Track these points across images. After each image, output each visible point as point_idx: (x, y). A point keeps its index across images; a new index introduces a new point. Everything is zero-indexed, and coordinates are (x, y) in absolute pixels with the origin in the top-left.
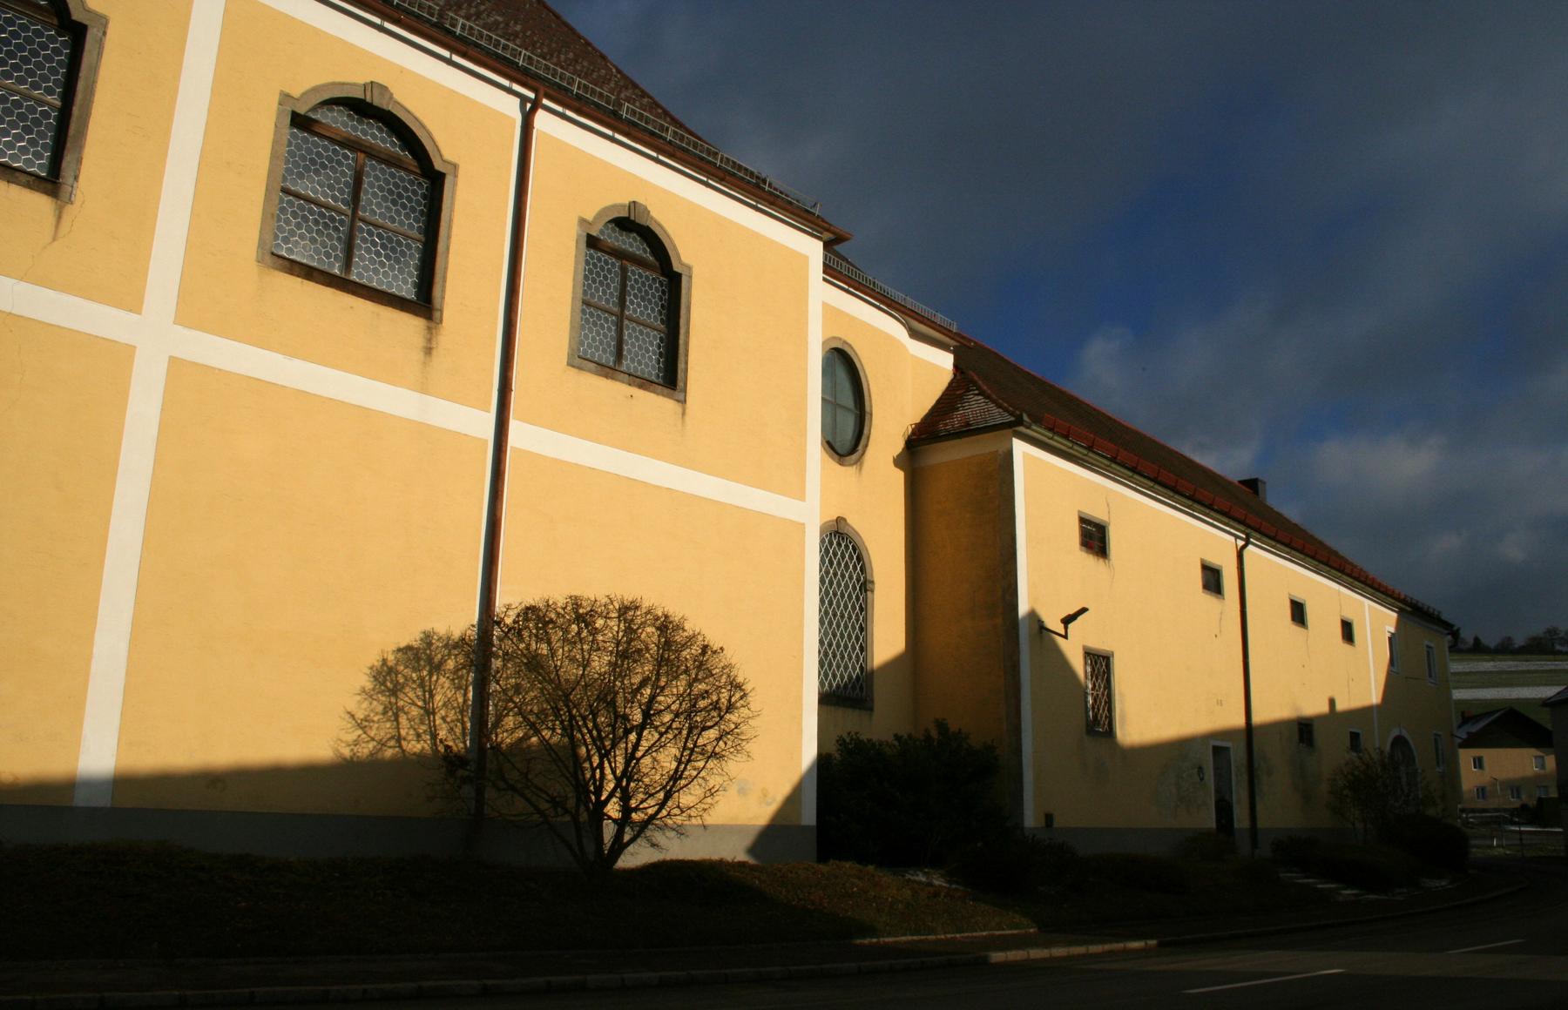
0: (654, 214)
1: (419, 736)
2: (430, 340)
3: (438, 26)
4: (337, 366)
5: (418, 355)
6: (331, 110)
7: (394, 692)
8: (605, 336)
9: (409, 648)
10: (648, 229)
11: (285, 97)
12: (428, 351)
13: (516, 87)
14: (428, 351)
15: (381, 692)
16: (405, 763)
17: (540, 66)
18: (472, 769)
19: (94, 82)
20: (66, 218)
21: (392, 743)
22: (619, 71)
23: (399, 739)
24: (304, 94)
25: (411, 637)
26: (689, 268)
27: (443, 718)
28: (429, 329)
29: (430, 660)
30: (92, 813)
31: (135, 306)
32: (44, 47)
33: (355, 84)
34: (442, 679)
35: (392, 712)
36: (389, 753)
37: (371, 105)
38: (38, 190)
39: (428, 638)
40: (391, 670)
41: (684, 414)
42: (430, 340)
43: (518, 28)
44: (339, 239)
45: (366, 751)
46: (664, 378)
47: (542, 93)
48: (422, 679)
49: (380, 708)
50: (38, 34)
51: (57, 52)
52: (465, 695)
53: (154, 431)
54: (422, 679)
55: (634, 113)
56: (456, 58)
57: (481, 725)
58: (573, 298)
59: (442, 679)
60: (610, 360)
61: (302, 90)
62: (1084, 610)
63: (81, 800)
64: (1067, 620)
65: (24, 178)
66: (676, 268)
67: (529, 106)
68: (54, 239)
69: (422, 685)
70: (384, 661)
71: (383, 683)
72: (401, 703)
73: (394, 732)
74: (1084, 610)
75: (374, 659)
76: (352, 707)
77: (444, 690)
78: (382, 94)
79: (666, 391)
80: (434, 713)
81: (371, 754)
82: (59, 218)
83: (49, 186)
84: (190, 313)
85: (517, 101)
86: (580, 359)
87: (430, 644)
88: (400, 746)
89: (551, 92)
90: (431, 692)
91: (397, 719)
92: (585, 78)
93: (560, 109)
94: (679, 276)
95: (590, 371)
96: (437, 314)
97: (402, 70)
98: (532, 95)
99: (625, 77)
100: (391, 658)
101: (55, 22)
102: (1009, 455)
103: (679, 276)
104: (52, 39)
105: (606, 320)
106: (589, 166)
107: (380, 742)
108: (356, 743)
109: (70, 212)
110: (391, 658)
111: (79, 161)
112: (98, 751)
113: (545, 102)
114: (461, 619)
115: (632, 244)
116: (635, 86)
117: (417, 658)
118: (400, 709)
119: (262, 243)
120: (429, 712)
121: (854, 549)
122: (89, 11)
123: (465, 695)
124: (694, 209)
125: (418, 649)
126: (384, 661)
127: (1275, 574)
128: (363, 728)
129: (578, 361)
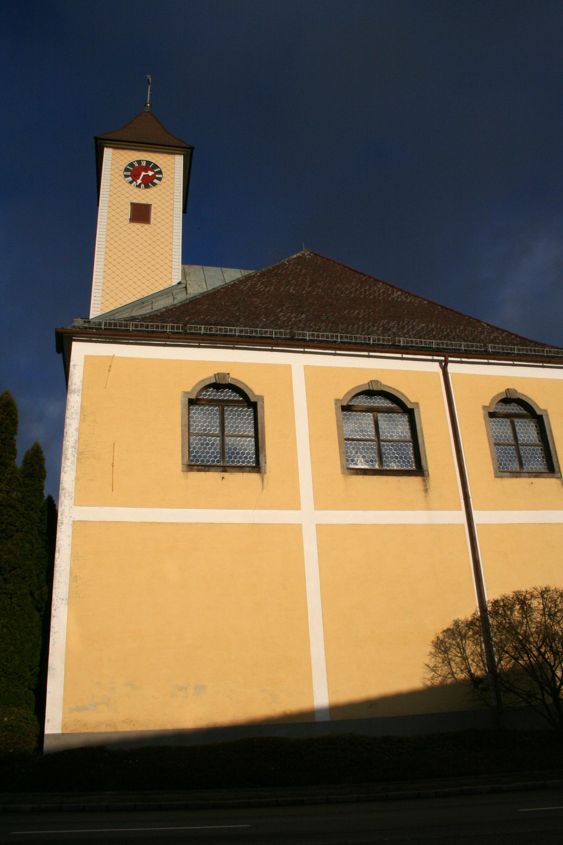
0: (520, 391)
1: (462, 670)
2: (425, 486)
5: (421, 494)
6: (358, 399)
7: (446, 651)
8: (512, 457)
9: (449, 630)
10: (519, 399)
11: (337, 401)
12: (426, 490)
13: (435, 358)
14: (426, 490)
15: (440, 653)
16: (457, 684)
17: (445, 344)
18: (488, 687)
19: (264, 423)
21: (450, 676)
22: (488, 325)
23: (453, 674)
25: (448, 624)
26: (545, 411)
27: (473, 660)
28: (424, 481)
29: (460, 633)
30: (324, 724)
31: (298, 507)
32: (244, 415)
33: (364, 385)
34: (468, 642)
35: (448, 661)
36: (449, 681)
37: (373, 391)
38: (254, 472)
39: (456, 623)
40: (442, 642)
42: (425, 486)
43: (433, 325)
44: (375, 453)
45: (438, 682)
46: (548, 468)
47: (447, 356)
48: (458, 643)
49: (441, 660)
50: (241, 411)
51: (249, 415)
52: (481, 647)
53: (316, 557)
54: (458, 643)
55: (495, 347)
57: (491, 664)
59: (468, 642)
60: (516, 466)
61: (343, 395)
63: (318, 719)
65: (247, 469)
66: (539, 413)
67: (443, 364)
68: (263, 489)
69: (458, 646)
70: (438, 638)
71: (440, 648)
72: (450, 656)
73: (449, 671)
75: (433, 638)
76: (427, 662)
77: (470, 647)
78: (376, 384)
79: (549, 475)
80: (467, 659)
81: (441, 683)
83: (257, 469)
84: (321, 503)
85: (438, 364)
86: (502, 470)
87: (458, 626)
88: (454, 677)
89: (451, 354)
90: (463, 649)
91: (450, 664)
94: (541, 417)
95: (507, 477)
96: (426, 473)
97: (383, 370)
98: (443, 358)
99: (492, 327)
100: (441, 636)
101: (246, 404)
103: (541, 417)
104: (246, 411)
105: (510, 450)
106: (482, 379)
107: (444, 676)
108: (432, 678)
109: (266, 477)
110: (441, 636)
111: (265, 455)
112: (321, 698)
113: (450, 359)
115: (514, 409)
116: (498, 329)
117: (454, 634)
118: (451, 659)
119: (342, 466)
120: (465, 659)
122: (256, 396)
123: (481, 647)
124: (539, 381)
125: (453, 629)
126: (438, 638)
128: (434, 671)
129: (500, 474)
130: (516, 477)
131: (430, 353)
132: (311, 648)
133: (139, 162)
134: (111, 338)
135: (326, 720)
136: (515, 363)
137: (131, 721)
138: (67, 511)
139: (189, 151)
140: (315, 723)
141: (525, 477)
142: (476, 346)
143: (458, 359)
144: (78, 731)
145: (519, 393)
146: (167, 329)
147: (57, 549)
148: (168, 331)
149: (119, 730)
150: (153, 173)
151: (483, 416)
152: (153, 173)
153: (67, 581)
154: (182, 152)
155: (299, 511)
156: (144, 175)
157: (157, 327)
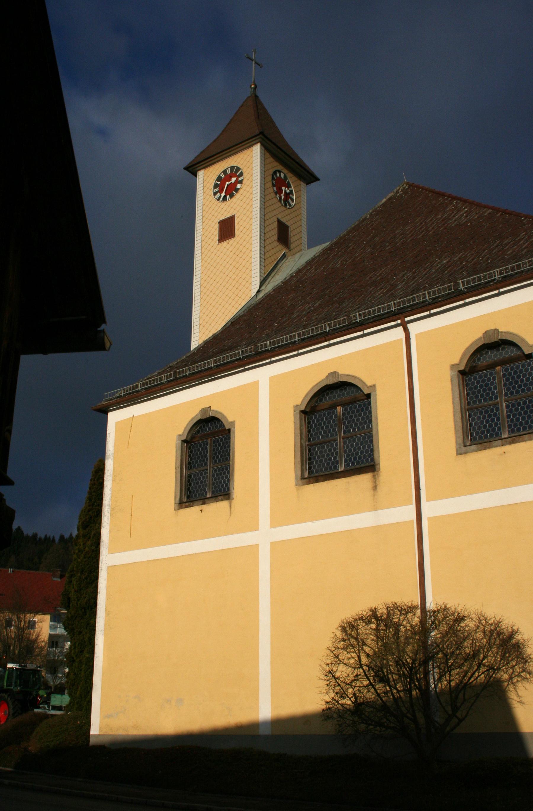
0: (502, 329)
2: (375, 482)
3: (258, 354)
4: (345, 512)
12: (375, 488)
20: (232, 506)
28: (374, 476)
30: (265, 737)
42: (375, 482)
56: (301, 351)
63: (263, 731)
82: (231, 506)
92: (298, 328)
93: (462, 302)
95: (473, 451)
97: (341, 358)
109: (234, 502)
112: (265, 711)
113: (407, 319)
129: (464, 449)
130: (485, 449)
131: (425, 308)
132: (260, 665)
133: (225, 172)
134: (132, 401)
135: (266, 733)
136: (501, 290)
137: (137, 727)
138: (104, 559)
139: (261, 136)
140: (259, 736)
141: (497, 446)
142: (442, 289)
143: (427, 313)
144: (108, 733)
145: (502, 332)
146: (495, 276)
147: (99, 591)
148: (497, 277)
149: (130, 733)
150: (235, 178)
151: (449, 379)
152: (235, 178)
153: (104, 616)
154: (257, 141)
155: (257, 532)
156: (228, 185)
157: (513, 269)
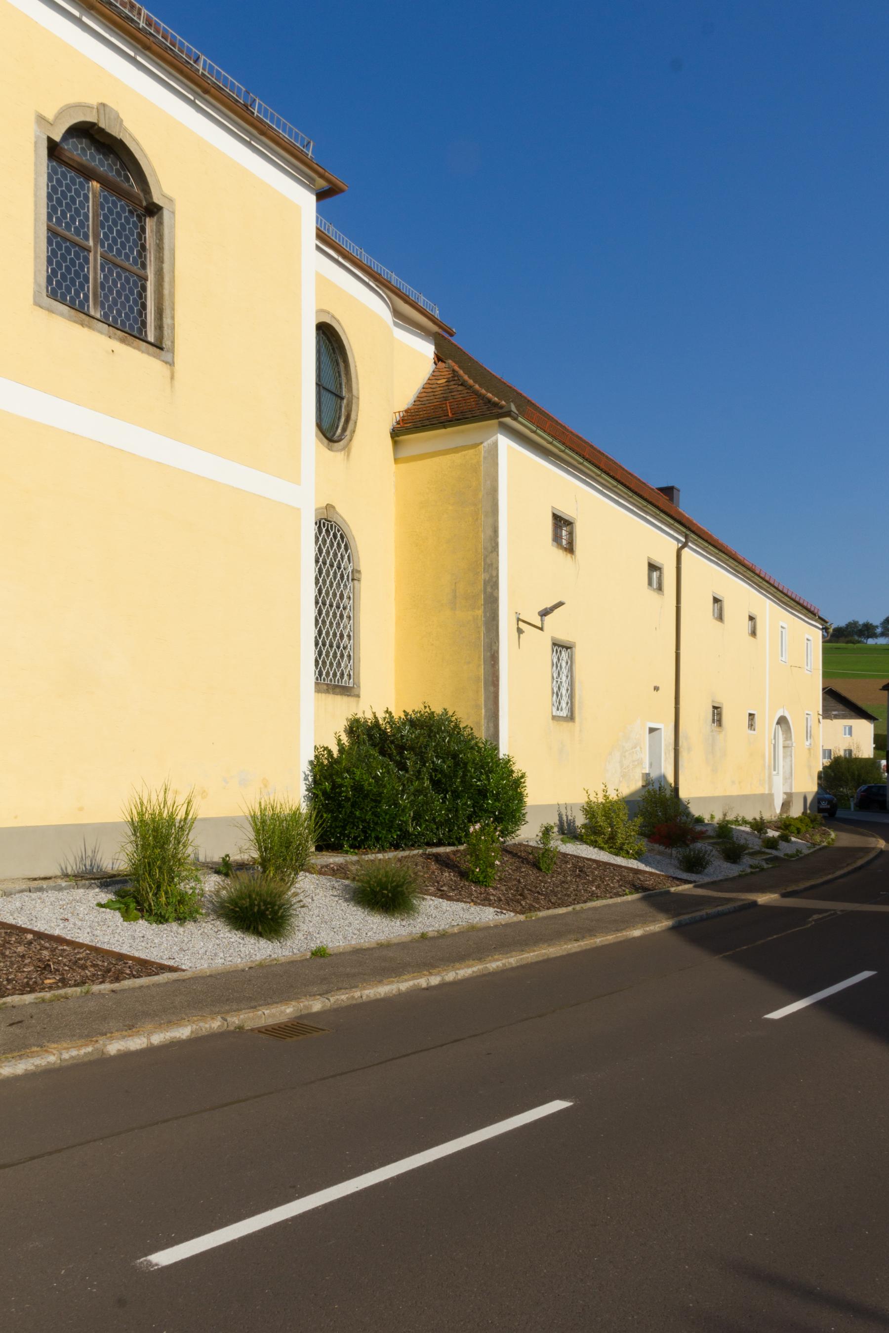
0: (126, 124)
10: (121, 143)
24: (252, 1030)
41: (172, 377)
58: (36, 257)
62: (561, 604)
64: (544, 613)
74: (561, 604)
95: (62, 315)
102: (495, 445)
114: (820, 632)
121: (342, 537)
127: (704, 574)
